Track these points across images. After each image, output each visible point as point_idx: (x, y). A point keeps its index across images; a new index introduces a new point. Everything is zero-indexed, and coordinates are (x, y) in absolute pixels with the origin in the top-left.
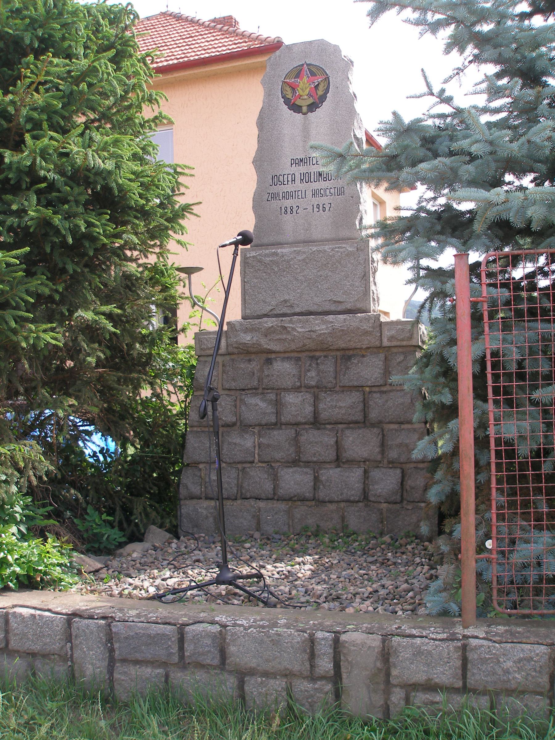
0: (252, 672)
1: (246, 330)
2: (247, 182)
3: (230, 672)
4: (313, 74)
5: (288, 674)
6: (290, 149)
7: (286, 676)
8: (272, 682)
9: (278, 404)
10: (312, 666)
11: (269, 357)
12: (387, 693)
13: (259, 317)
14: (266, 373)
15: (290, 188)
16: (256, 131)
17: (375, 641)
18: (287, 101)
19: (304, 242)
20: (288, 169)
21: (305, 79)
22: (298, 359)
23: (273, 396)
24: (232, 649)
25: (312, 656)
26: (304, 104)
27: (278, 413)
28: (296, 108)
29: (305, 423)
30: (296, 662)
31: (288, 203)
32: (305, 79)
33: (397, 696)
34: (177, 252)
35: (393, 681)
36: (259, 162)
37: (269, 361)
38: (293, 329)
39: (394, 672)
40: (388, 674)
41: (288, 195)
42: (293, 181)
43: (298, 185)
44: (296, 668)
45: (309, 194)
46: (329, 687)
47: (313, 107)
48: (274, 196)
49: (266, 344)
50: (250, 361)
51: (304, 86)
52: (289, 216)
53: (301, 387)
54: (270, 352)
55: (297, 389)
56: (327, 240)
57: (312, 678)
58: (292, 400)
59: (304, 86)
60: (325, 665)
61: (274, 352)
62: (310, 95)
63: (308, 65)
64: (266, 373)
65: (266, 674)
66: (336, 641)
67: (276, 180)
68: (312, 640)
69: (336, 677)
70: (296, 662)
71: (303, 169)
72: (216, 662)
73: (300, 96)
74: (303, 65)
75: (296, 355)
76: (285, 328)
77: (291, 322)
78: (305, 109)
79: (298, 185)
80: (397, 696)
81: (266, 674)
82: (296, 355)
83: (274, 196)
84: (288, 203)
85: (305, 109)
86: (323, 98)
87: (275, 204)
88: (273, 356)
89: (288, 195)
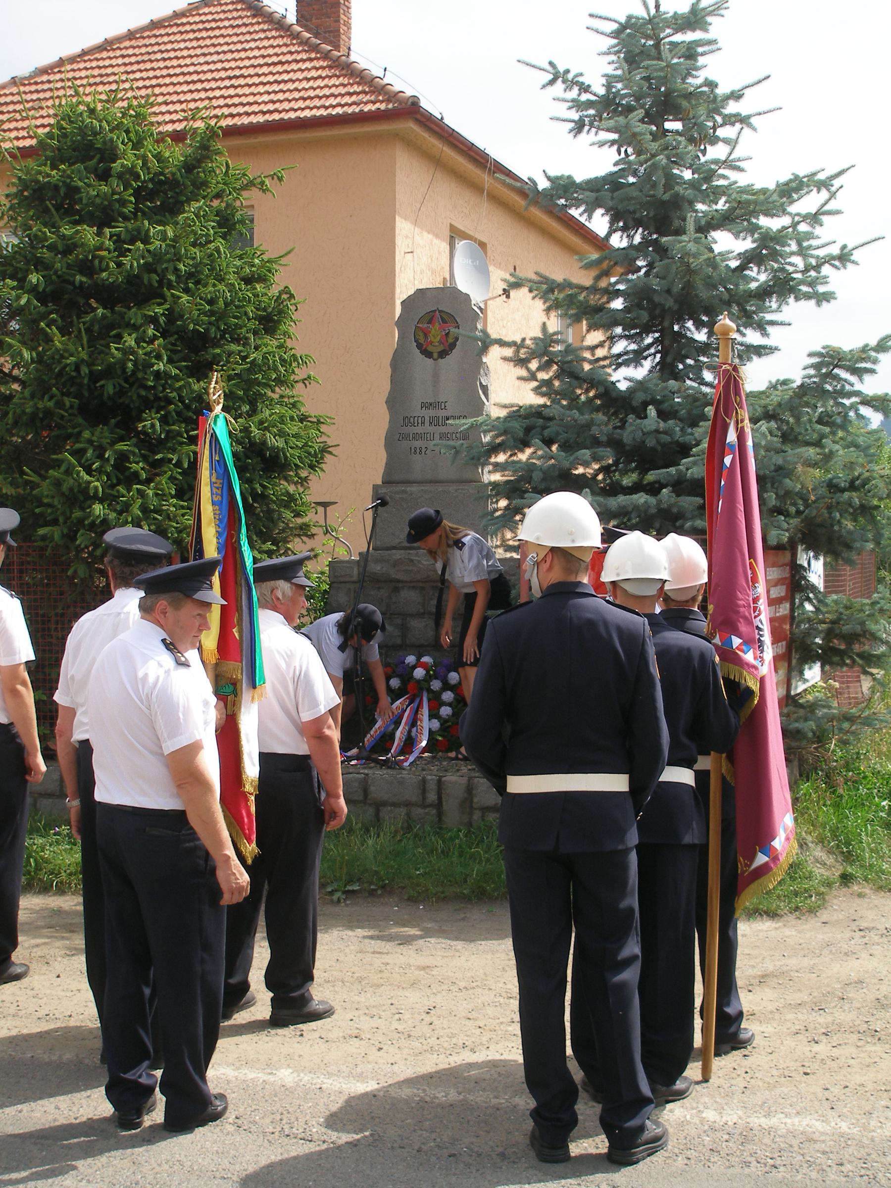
0: (384, 804)
1: (377, 561)
2: (380, 421)
3: (370, 805)
4: (444, 321)
5: (408, 804)
6: (420, 393)
7: (407, 805)
8: (398, 810)
9: (404, 628)
10: (424, 799)
11: (396, 586)
12: (471, 814)
13: (388, 549)
14: (394, 600)
15: (419, 430)
16: (389, 370)
17: (464, 781)
18: (419, 346)
19: (431, 482)
20: (418, 412)
21: (437, 326)
22: (423, 588)
23: (399, 621)
24: (372, 788)
25: (424, 791)
26: (435, 349)
27: (403, 636)
28: (428, 354)
29: (427, 646)
30: (412, 795)
31: (418, 444)
32: (437, 326)
33: (477, 815)
34: (318, 487)
35: (475, 806)
36: (392, 402)
37: (396, 590)
38: (419, 562)
39: (475, 800)
40: (471, 802)
41: (417, 437)
42: (423, 423)
43: (427, 428)
44: (414, 799)
45: (437, 436)
46: (434, 811)
47: (443, 354)
48: (406, 437)
49: (394, 574)
50: (379, 588)
51: (436, 332)
52: (418, 456)
53: (423, 614)
54: (398, 581)
55: (420, 615)
56: (452, 482)
57: (424, 806)
58: (416, 624)
59: (436, 332)
60: (432, 797)
61: (402, 582)
62: (440, 342)
63: (440, 311)
64: (394, 600)
65: (395, 805)
66: (440, 782)
67: (407, 421)
68: (424, 781)
69: (439, 805)
70: (412, 795)
71: (432, 413)
72: (361, 798)
73: (431, 342)
74: (434, 311)
75: (421, 584)
76: (412, 561)
77: (417, 555)
78: (435, 355)
79: (427, 428)
80: (477, 815)
81: (395, 805)
82: (421, 584)
83: (406, 437)
84: (418, 444)
85: (435, 355)
86: (453, 346)
87: (405, 444)
88: (400, 585)
89: (417, 437)
